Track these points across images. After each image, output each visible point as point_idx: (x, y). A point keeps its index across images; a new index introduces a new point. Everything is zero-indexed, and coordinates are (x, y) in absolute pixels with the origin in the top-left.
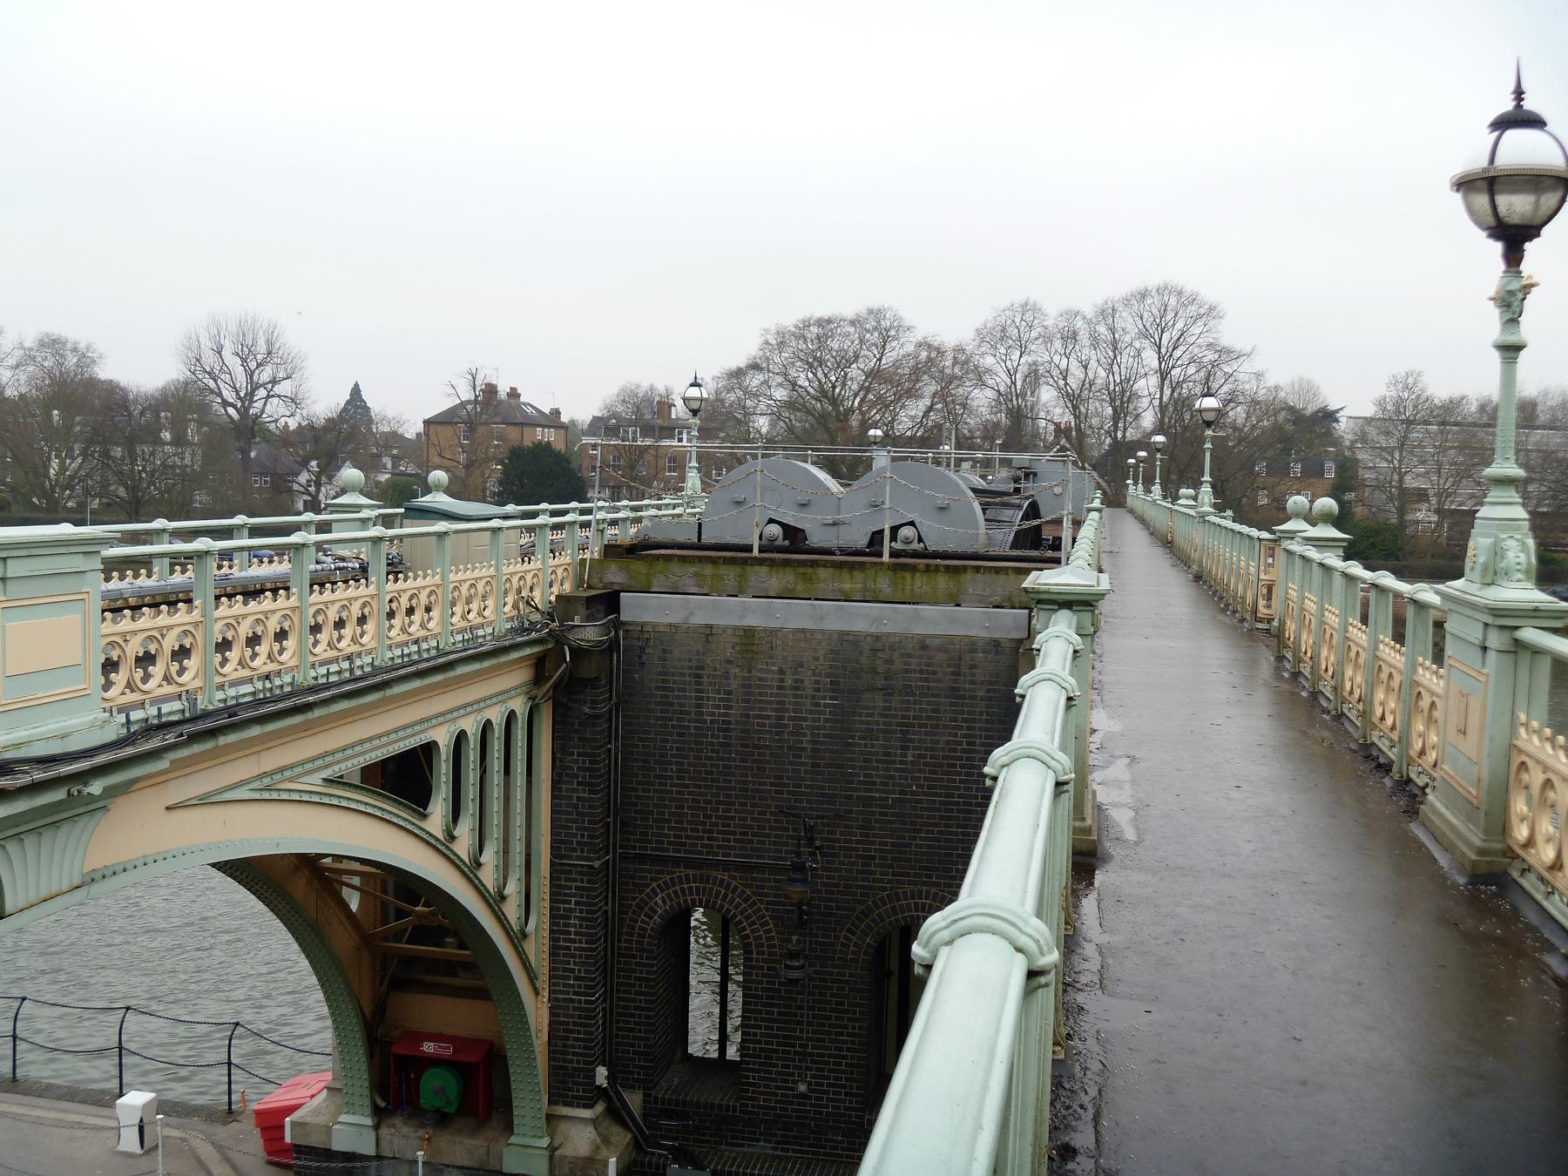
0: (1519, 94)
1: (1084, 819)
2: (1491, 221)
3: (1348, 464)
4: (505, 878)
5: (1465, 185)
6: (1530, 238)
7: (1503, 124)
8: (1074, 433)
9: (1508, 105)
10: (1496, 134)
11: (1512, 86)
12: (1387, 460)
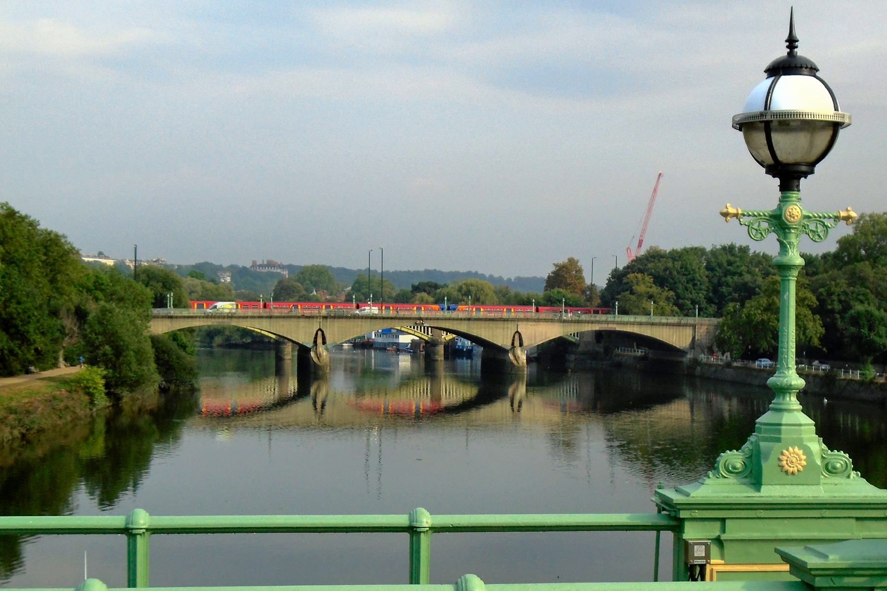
0: (792, 42)
1: (838, 111)
2: (770, 160)
3: (320, 285)
4: (695, 332)
5: (745, 125)
6: (805, 175)
7: (777, 70)
8: (446, 299)
9: (782, 52)
10: (772, 79)
11: (786, 36)
12: (75, 344)
